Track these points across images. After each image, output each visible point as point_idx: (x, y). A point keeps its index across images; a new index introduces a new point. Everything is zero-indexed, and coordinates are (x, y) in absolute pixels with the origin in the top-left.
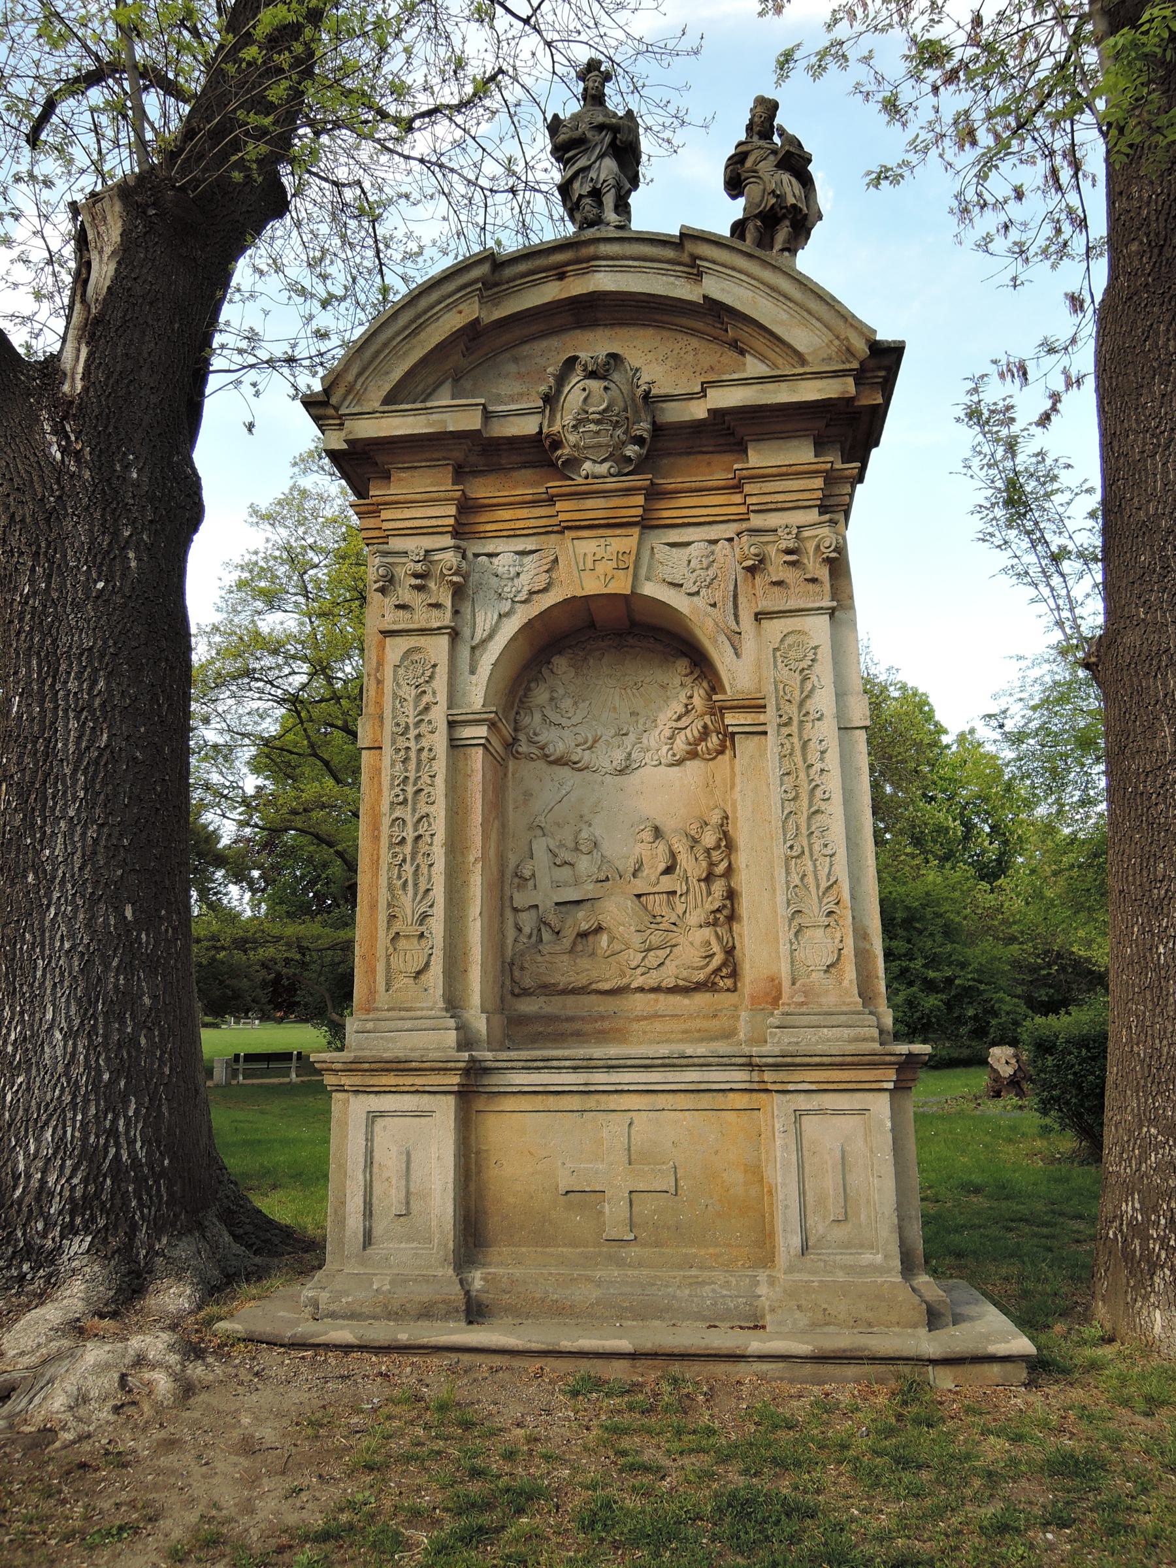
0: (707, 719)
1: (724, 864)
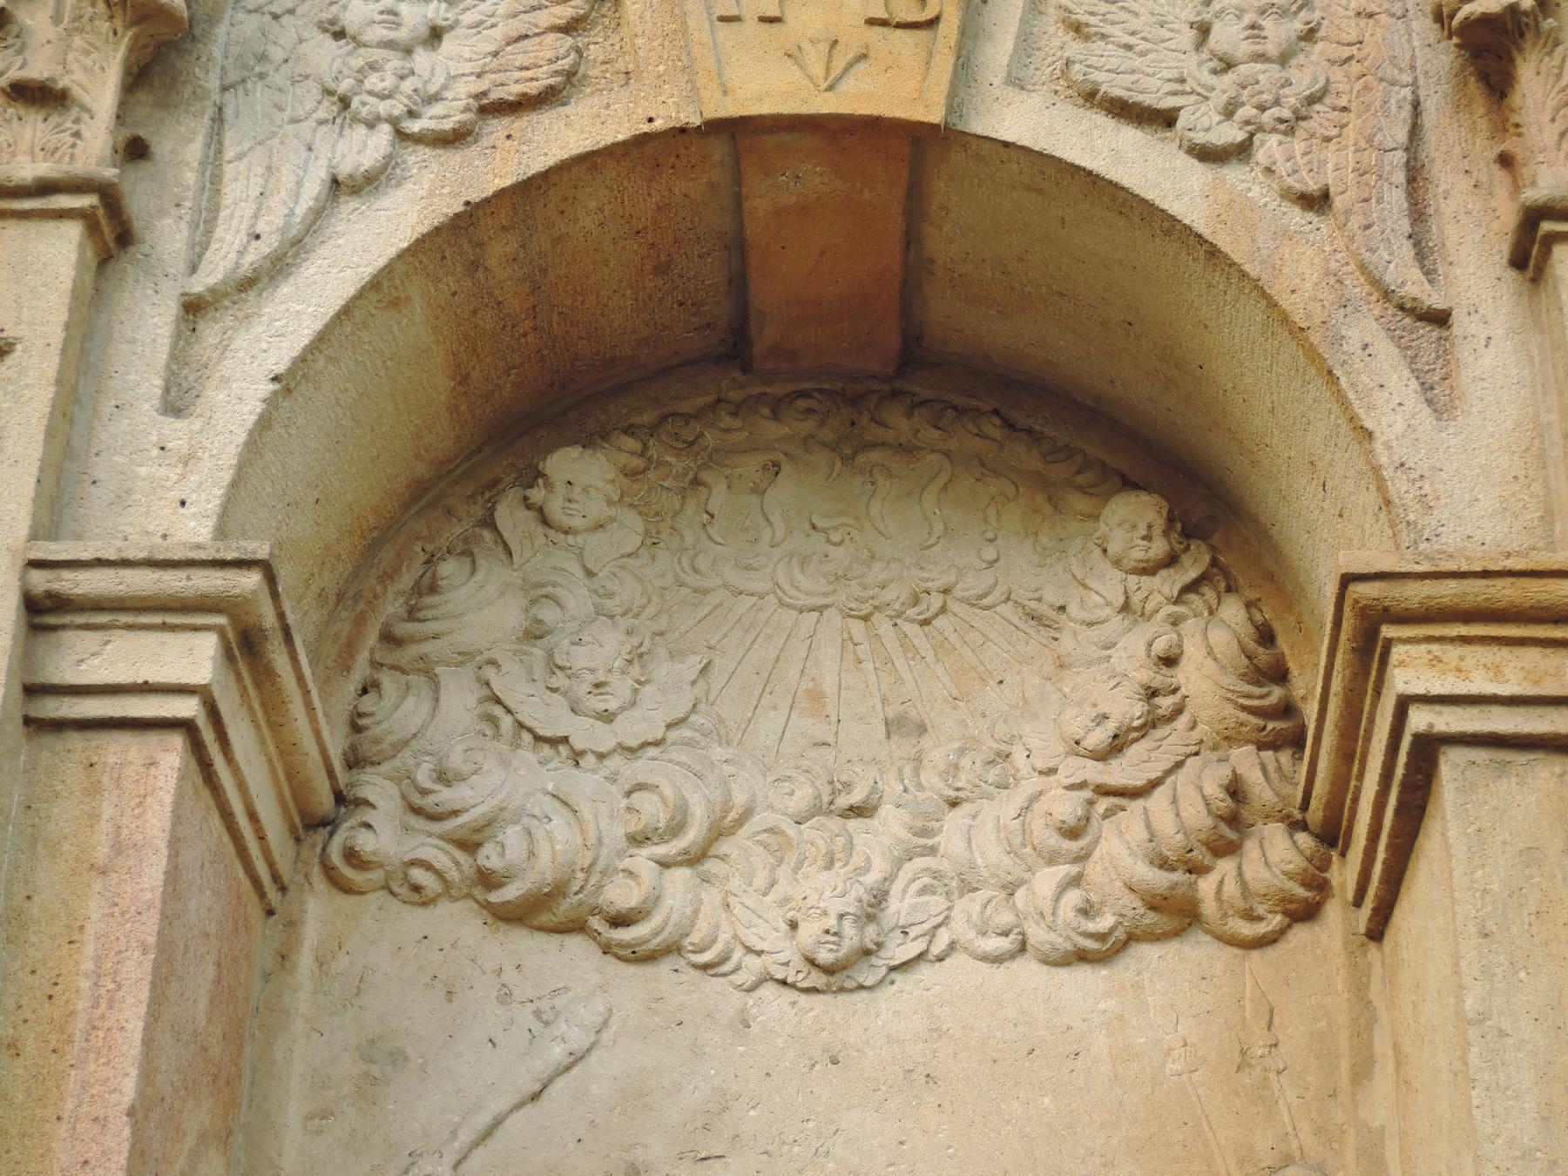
0: (1245, 760)
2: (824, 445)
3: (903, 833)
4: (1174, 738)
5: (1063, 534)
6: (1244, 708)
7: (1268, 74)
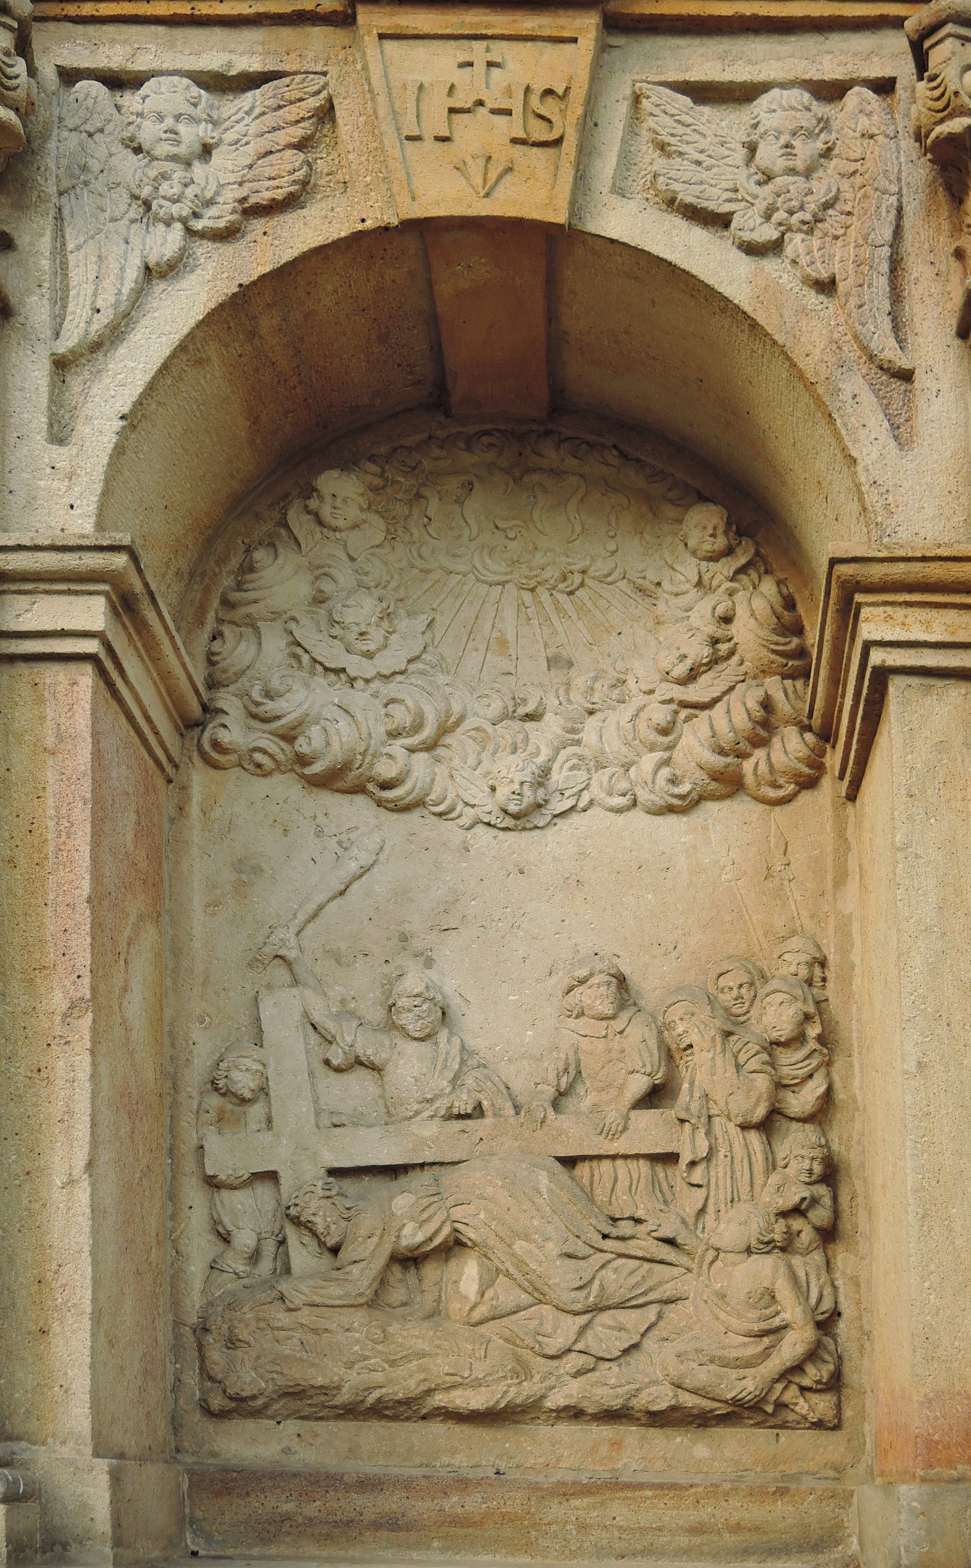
0: (774, 686)
2: (501, 469)
3: (560, 732)
4: (729, 671)
5: (660, 533)
6: (774, 651)
7: (796, 184)
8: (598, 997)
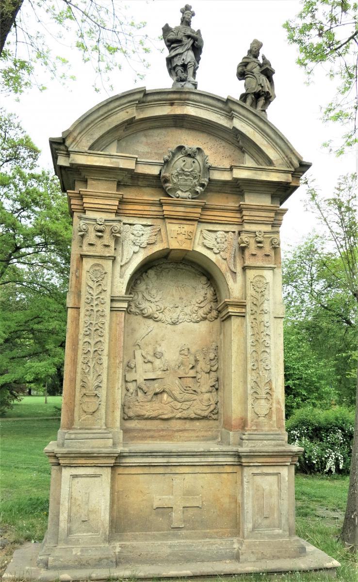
1: (216, 367)
4: (206, 302)
8: (186, 352)
